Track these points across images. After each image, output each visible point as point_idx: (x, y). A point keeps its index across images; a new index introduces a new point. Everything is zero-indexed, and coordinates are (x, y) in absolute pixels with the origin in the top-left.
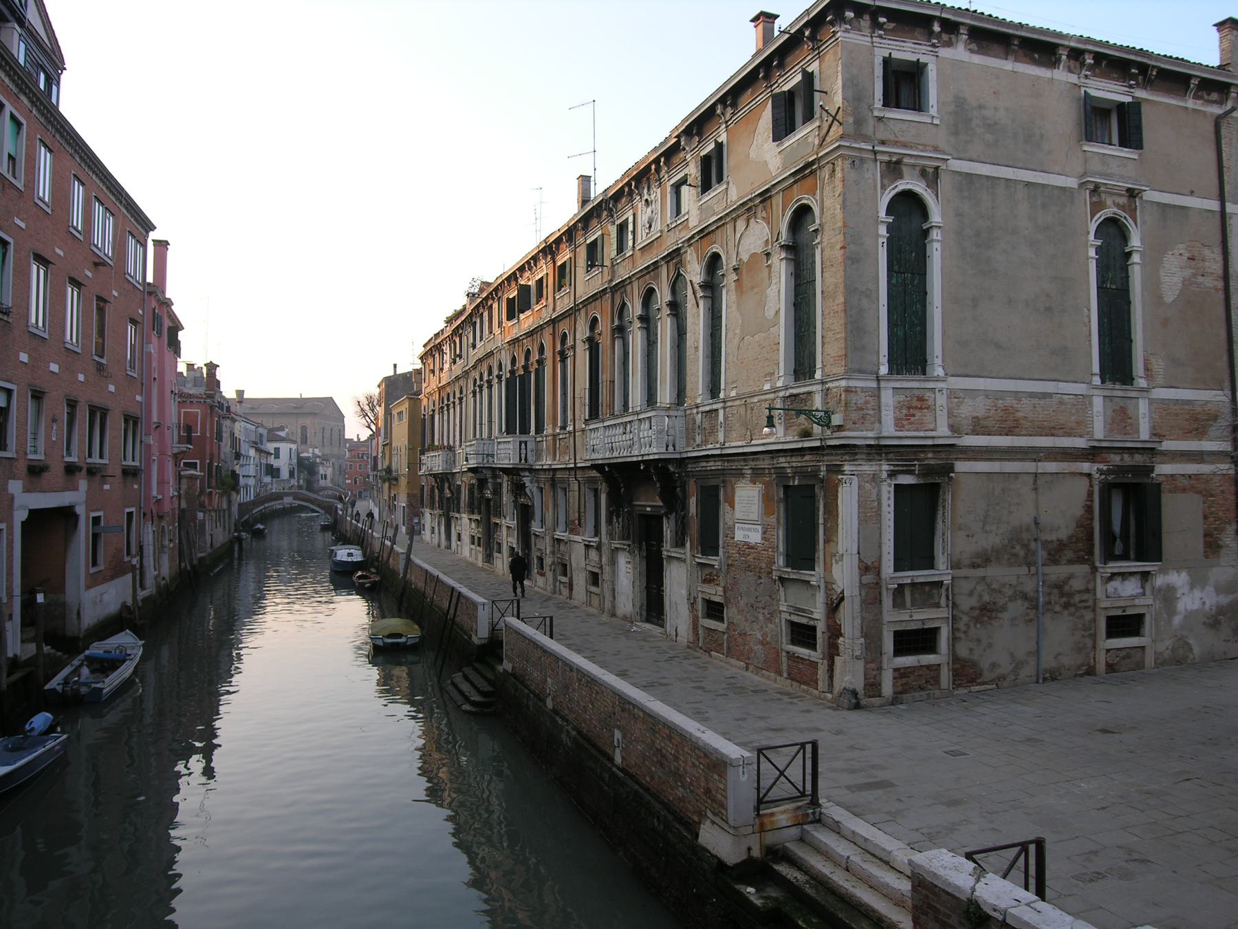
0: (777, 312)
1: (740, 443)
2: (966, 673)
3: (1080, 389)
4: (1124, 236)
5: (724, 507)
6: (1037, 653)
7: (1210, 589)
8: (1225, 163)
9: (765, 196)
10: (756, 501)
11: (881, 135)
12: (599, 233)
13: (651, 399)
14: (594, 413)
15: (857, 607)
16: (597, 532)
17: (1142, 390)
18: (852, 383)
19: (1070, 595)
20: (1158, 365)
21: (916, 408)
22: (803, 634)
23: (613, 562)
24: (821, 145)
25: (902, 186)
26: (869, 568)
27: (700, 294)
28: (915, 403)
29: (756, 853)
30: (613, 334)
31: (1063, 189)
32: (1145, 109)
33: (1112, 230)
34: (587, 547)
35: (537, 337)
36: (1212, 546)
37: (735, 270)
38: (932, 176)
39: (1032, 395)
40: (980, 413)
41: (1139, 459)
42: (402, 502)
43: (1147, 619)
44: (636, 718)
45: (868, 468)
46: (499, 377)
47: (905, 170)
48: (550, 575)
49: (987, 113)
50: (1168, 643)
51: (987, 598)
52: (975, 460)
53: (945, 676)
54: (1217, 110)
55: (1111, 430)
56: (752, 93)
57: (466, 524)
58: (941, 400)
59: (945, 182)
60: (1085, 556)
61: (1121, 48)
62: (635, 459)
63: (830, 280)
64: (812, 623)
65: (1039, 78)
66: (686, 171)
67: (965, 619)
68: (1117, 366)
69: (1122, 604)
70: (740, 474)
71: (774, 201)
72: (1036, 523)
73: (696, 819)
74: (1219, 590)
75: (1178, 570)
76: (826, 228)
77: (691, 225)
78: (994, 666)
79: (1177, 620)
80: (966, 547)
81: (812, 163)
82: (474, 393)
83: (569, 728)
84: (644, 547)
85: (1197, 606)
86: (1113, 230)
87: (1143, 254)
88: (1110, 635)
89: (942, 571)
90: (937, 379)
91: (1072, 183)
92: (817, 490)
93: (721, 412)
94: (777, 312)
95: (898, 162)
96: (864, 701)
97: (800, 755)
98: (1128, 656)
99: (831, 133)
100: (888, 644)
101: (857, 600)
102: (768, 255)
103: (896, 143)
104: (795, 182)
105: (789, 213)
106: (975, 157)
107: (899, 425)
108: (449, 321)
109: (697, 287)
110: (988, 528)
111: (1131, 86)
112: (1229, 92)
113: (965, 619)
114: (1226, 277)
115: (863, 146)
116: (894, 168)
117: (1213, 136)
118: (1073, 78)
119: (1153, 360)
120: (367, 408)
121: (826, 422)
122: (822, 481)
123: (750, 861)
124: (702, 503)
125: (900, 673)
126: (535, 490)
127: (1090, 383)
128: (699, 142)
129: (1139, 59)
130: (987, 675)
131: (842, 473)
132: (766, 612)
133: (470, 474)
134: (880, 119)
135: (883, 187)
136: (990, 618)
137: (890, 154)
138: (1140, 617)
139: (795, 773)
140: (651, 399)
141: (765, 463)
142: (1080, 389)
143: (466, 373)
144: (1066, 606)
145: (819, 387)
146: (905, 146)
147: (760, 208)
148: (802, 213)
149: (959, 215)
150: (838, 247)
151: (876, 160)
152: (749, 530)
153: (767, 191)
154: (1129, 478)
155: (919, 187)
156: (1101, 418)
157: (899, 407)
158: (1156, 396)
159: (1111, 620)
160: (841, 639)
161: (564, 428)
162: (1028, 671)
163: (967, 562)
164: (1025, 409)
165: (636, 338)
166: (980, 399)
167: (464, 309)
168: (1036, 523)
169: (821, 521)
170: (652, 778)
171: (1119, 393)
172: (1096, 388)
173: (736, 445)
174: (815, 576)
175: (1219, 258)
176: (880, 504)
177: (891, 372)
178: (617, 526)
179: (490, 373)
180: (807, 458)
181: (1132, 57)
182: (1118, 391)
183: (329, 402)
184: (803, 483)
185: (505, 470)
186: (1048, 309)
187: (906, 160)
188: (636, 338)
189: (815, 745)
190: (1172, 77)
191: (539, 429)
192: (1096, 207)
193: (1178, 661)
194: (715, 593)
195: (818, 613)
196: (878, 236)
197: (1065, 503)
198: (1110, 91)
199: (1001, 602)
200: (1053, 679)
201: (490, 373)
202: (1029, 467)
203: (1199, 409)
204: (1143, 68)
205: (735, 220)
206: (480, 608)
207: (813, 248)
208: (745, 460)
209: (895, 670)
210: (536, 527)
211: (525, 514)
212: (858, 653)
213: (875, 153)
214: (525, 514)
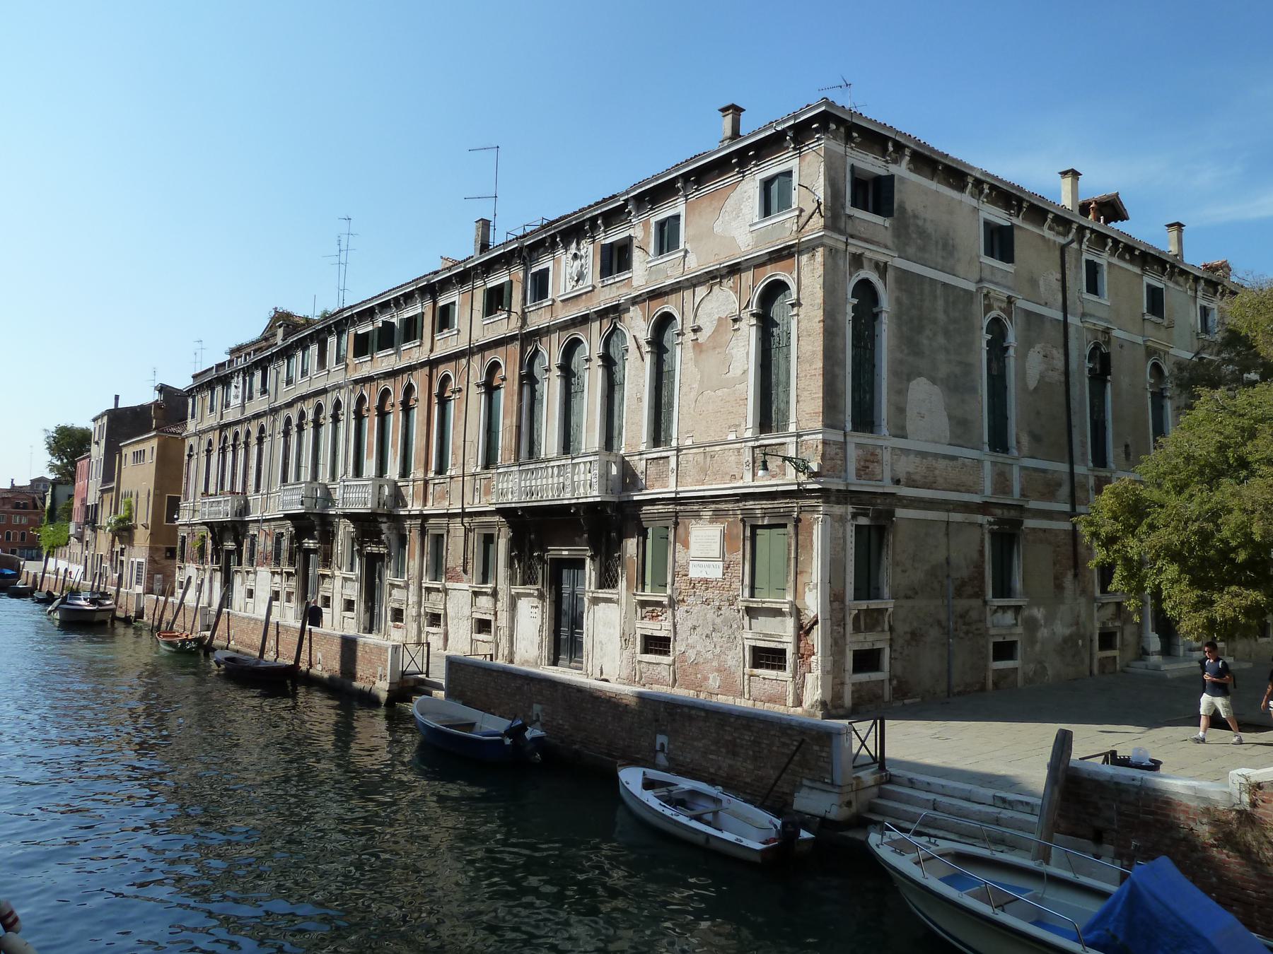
12: (507, 279)
20: (1025, 440)
32: (1016, 232)
34: (476, 594)
35: (403, 380)
38: (882, 269)
47: (866, 263)
49: (920, 223)
54: (1062, 240)
59: (890, 275)
61: (1008, 184)
62: (566, 502)
64: (780, 646)
66: (631, 232)
68: (999, 441)
69: (1004, 632)
77: (635, 284)
86: (997, 327)
87: (1016, 351)
93: (673, 461)
95: (861, 255)
100: (849, 664)
117: (1059, 261)
118: (974, 202)
135: (851, 275)
138: (1014, 643)
140: (567, 445)
142: (974, 454)
143: (274, 411)
148: (775, 289)
155: (874, 277)
175: (1062, 358)
182: (1001, 458)
190: (1037, 211)
198: (999, 216)
204: (1020, 200)
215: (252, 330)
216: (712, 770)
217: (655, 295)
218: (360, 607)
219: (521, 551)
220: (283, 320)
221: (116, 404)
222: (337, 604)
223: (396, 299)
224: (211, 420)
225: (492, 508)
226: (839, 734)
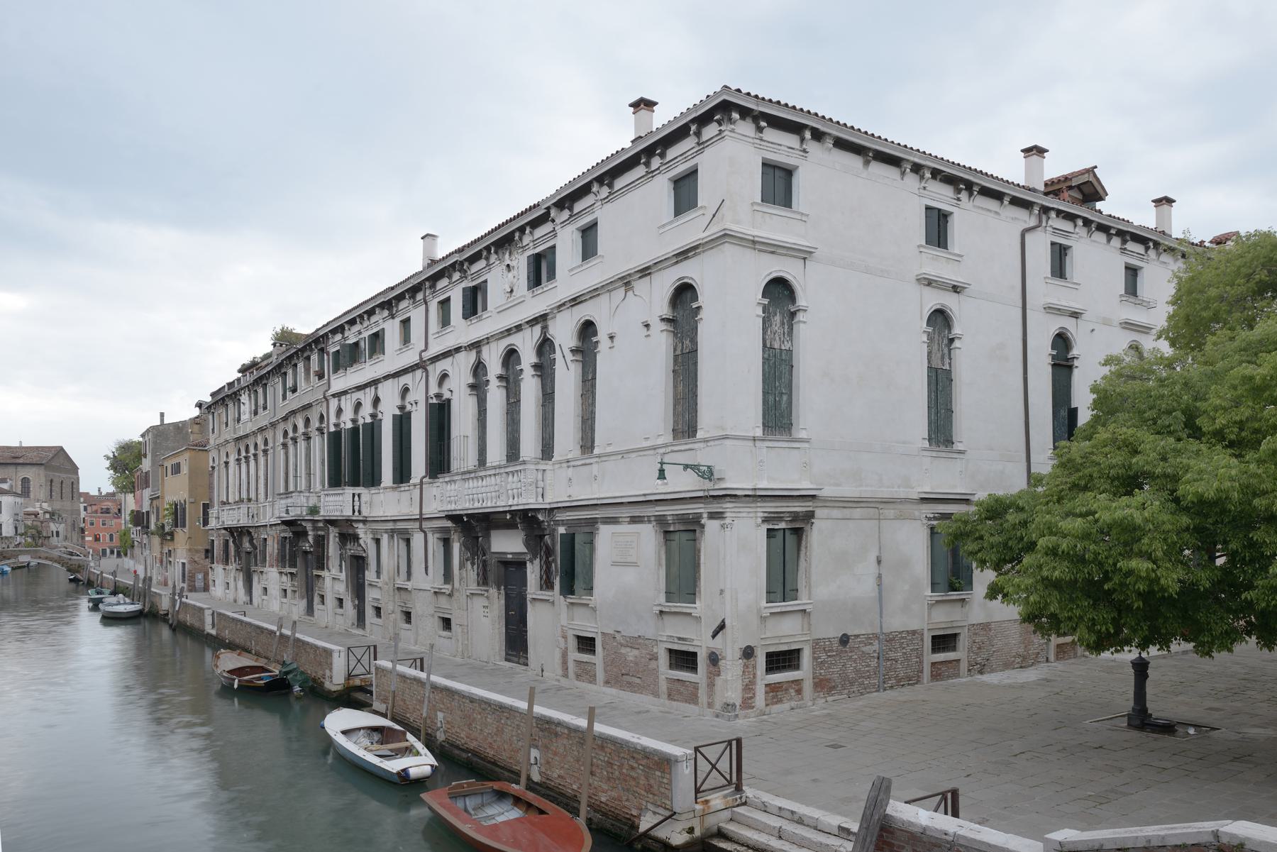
13: (547, 451)
16: (448, 577)
22: (684, 659)
27: (569, 357)
35: (291, 420)
42: (181, 557)
57: (272, 577)
64: (691, 649)
73: (635, 812)
82: (285, 445)
84: (503, 592)
97: (728, 751)
108: (244, 370)
125: (773, 689)
133: (284, 527)
139: (724, 765)
140: (547, 451)
143: (273, 425)
148: (684, 293)
159: (770, 656)
167: (267, 356)
179: (247, 451)
185: (332, 522)
201: (247, 451)
206: (335, 655)
210: (370, 575)
211: (358, 564)
214: (358, 564)
215: (261, 346)
216: (575, 787)
217: (576, 301)
218: (348, 604)
219: (473, 555)
220: (284, 338)
221: (162, 420)
222: (330, 601)
223: (361, 316)
224: (228, 434)
225: (443, 515)
226: (677, 761)
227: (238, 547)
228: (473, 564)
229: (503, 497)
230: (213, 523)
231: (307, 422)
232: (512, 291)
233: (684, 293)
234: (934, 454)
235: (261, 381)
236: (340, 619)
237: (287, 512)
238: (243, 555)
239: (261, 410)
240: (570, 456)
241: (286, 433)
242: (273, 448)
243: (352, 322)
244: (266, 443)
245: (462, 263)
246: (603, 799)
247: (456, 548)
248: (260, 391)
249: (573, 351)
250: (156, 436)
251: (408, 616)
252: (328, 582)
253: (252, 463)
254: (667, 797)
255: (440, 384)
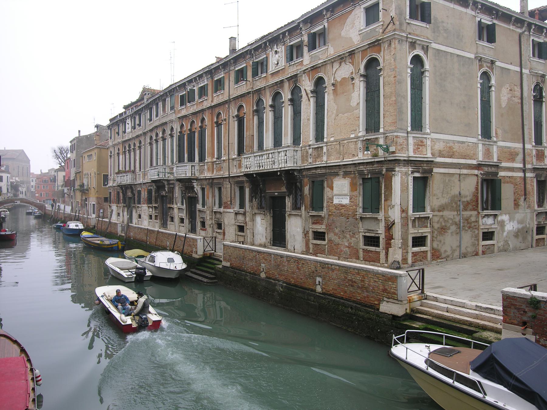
0: (358, 104)
1: (337, 161)
2: (436, 255)
3: (474, 140)
4: (489, 79)
5: (327, 190)
6: (460, 246)
7: (516, 222)
8: (522, 53)
9: (352, 54)
10: (346, 185)
11: (409, 30)
12: (245, 65)
14: (241, 151)
15: (400, 227)
16: (242, 206)
17: (495, 142)
18: (399, 134)
19: (471, 223)
20: (500, 132)
21: (420, 145)
23: (253, 220)
24: (383, 33)
25: (416, 52)
26: (404, 211)
27: (310, 95)
28: (420, 143)
29: (408, 311)
30: (253, 113)
31: (469, 58)
32: (497, 29)
33: (485, 77)
36: (517, 205)
37: (333, 85)
38: (426, 49)
39: (459, 142)
40: (441, 149)
41: (494, 170)
43: (496, 233)
44: (333, 270)
45: (404, 169)
46: (172, 136)
47: (417, 46)
48: (209, 230)
49: (445, 25)
50: (502, 243)
51: (443, 224)
52: (440, 167)
53: (429, 255)
54: (519, 31)
55: (484, 158)
56: (343, 7)
57: (145, 209)
58: (429, 143)
60: (475, 209)
63: (388, 90)
64: (377, 235)
65: (462, 12)
67: (436, 232)
68: (486, 133)
70: (337, 174)
71: (356, 56)
72: (460, 194)
73: (376, 303)
74: (519, 222)
75: (506, 214)
76: (386, 68)
77: (305, 63)
78: (445, 251)
79: (505, 234)
80: (436, 203)
81: (380, 40)
82: (151, 144)
83: (281, 283)
84: (272, 212)
85: (511, 228)
86: (486, 76)
88: (484, 240)
89: (428, 212)
90: (428, 134)
91: (472, 56)
92: (381, 179)
93: (325, 149)
94: (358, 104)
95: (415, 43)
96: (402, 266)
98: (489, 248)
99: (389, 27)
101: (400, 224)
102: (353, 79)
103: (414, 35)
104: (369, 48)
105: (365, 61)
106: (440, 43)
107: (415, 152)
109: (309, 92)
110: (444, 196)
111: (492, 18)
112: (524, 24)
113: (436, 232)
114: (522, 98)
115: (403, 34)
116: (413, 45)
117: (518, 41)
118: (473, 13)
119: (498, 130)
120: (59, 154)
121: (387, 150)
122: (383, 175)
123: (406, 315)
124: (312, 189)
125: (414, 254)
126: (199, 189)
127: (478, 138)
128: (311, 26)
129: (496, 7)
130: (443, 255)
131: (395, 171)
132: (351, 233)
134: (408, 23)
135: (409, 53)
136: (444, 232)
137: (413, 39)
139: (417, 281)
141: (352, 169)
142: (474, 140)
143: (145, 134)
144: (469, 228)
145: (382, 136)
146: (417, 36)
147: (348, 58)
148: (372, 63)
149: (435, 66)
150: (393, 76)
151: (407, 41)
152: (342, 198)
153: (354, 50)
154: (490, 177)
155: (421, 54)
156: (481, 152)
157: (415, 144)
158: (501, 143)
160: (393, 240)
161: (219, 157)
162: (457, 253)
163: (436, 209)
164: (456, 147)
165: (269, 117)
166: (441, 143)
168: (460, 194)
169: (383, 192)
170: (346, 292)
171: (487, 143)
172: (479, 140)
173: (334, 161)
174: (381, 215)
175: (520, 91)
176: (408, 185)
177: (412, 129)
178: (255, 203)
179: (125, 148)
180: (375, 166)
181: (494, 7)
183: (22, 152)
184: (373, 176)
186: (464, 107)
187: (418, 42)
188: (269, 117)
189: (423, 270)
191: (202, 159)
192: (481, 67)
193: (505, 250)
194: (321, 228)
195: (381, 231)
196: (408, 73)
197: (469, 186)
199: (448, 225)
200: (465, 257)
202: (457, 171)
203: (513, 151)
204: (497, 11)
205: (333, 63)
206: (199, 241)
207: (379, 77)
208: (339, 168)
209: (412, 253)
210: (199, 206)
212: (400, 246)
213: (407, 38)
218: (186, 221)
221: (79, 134)
222: (177, 220)
223: (195, 78)
224: (119, 140)
225: (242, 174)
227: (124, 194)
228: (256, 199)
229: (276, 164)
230: (111, 184)
231: (164, 131)
232: (278, 63)
233: (372, 63)
234: (483, 143)
235: (139, 113)
236: (182, 229)
237: (158, 175)
238: (127, 199)
239: (137, 127)
240: (310, 143)
241: (151, 138)
242: (114, 155)
243: (190, 81)
244: (140, 142)
245: (250, 50)
246: (359, 298)
247: (247, 191)
248: (137, 117)
249: (312, 92)
250: (77, 142)
251: (220, 226)
252: (176, 211)
253: (132, 153)
254: (395, 294)
255: (217, 118)
